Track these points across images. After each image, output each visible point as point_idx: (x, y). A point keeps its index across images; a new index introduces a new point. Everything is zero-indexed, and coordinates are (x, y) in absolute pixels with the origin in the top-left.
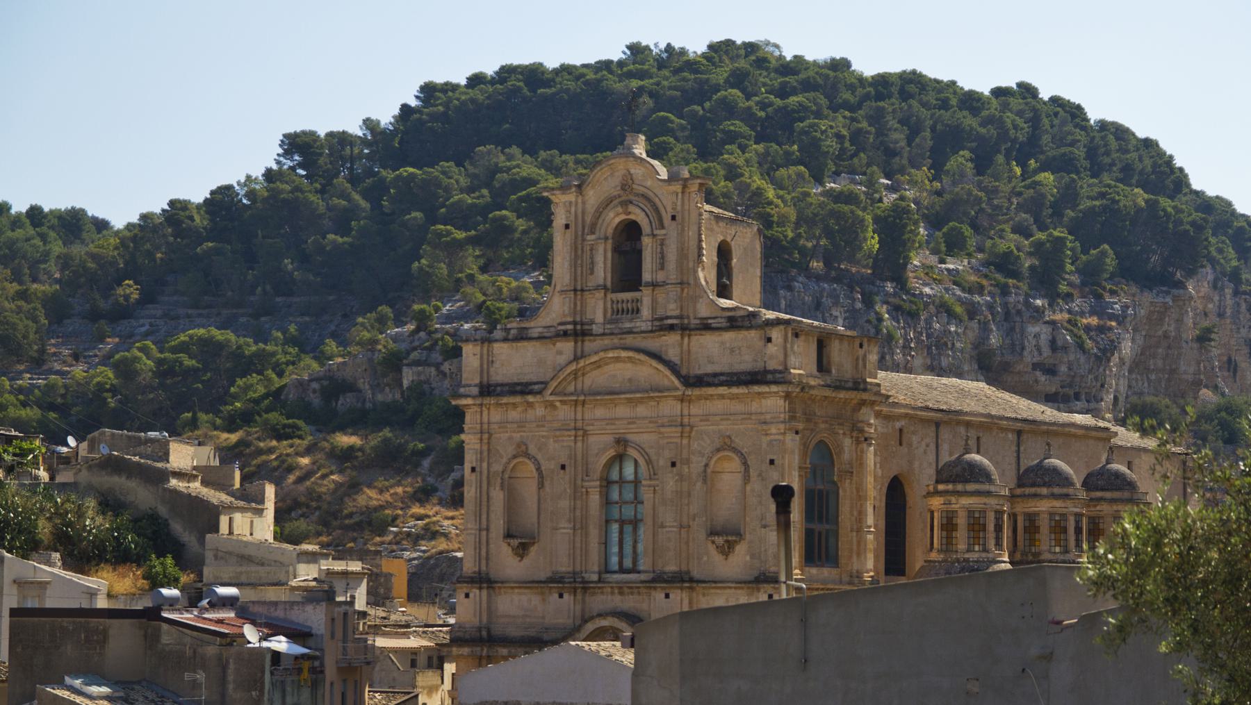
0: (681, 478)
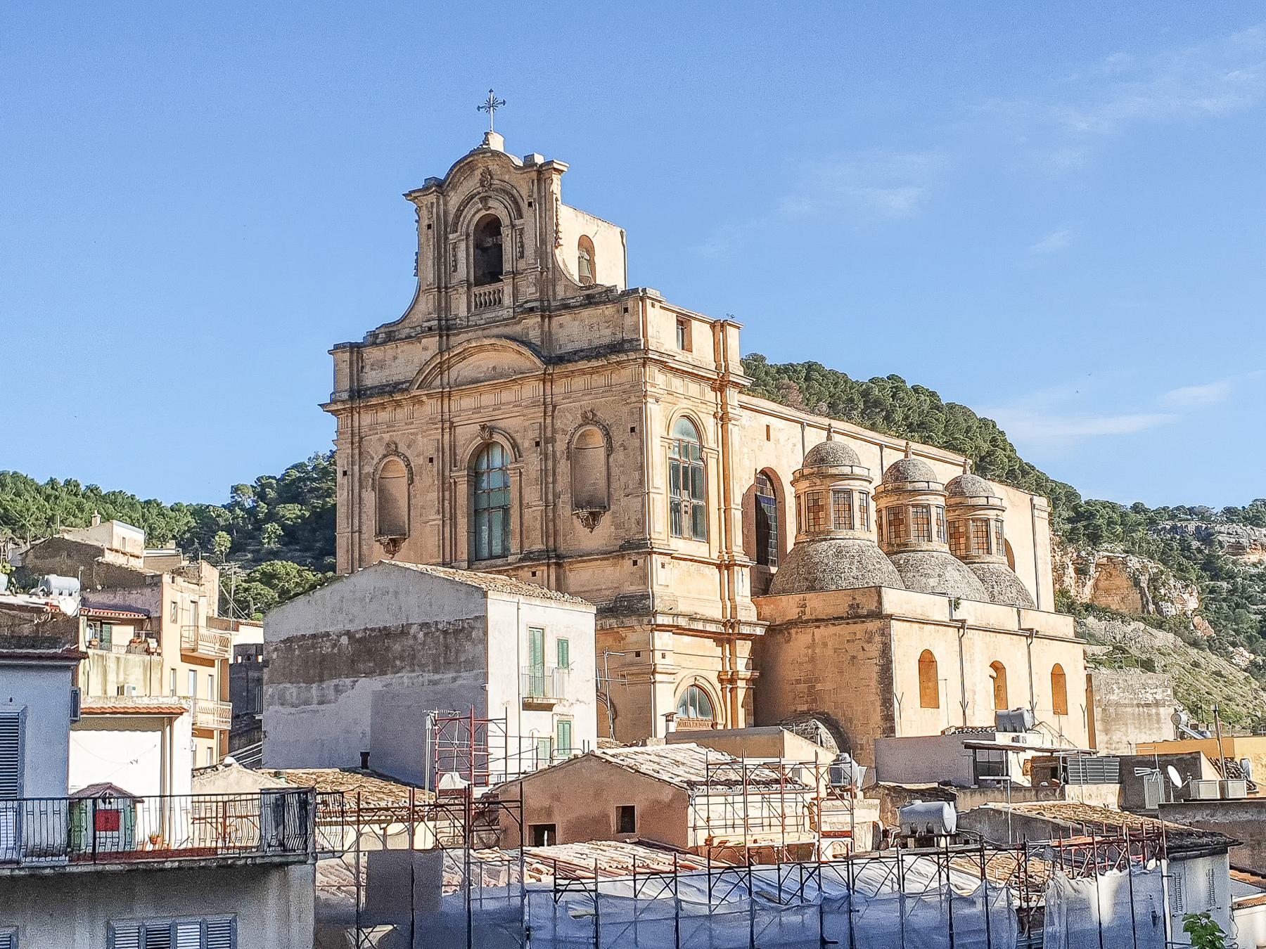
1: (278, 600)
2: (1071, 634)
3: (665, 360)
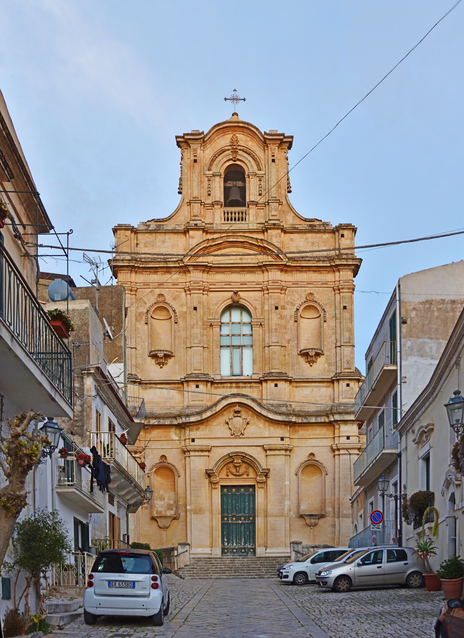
0: (281, 317)
1: (73, 551)
2: (229, 436)
3: (346, 284)
